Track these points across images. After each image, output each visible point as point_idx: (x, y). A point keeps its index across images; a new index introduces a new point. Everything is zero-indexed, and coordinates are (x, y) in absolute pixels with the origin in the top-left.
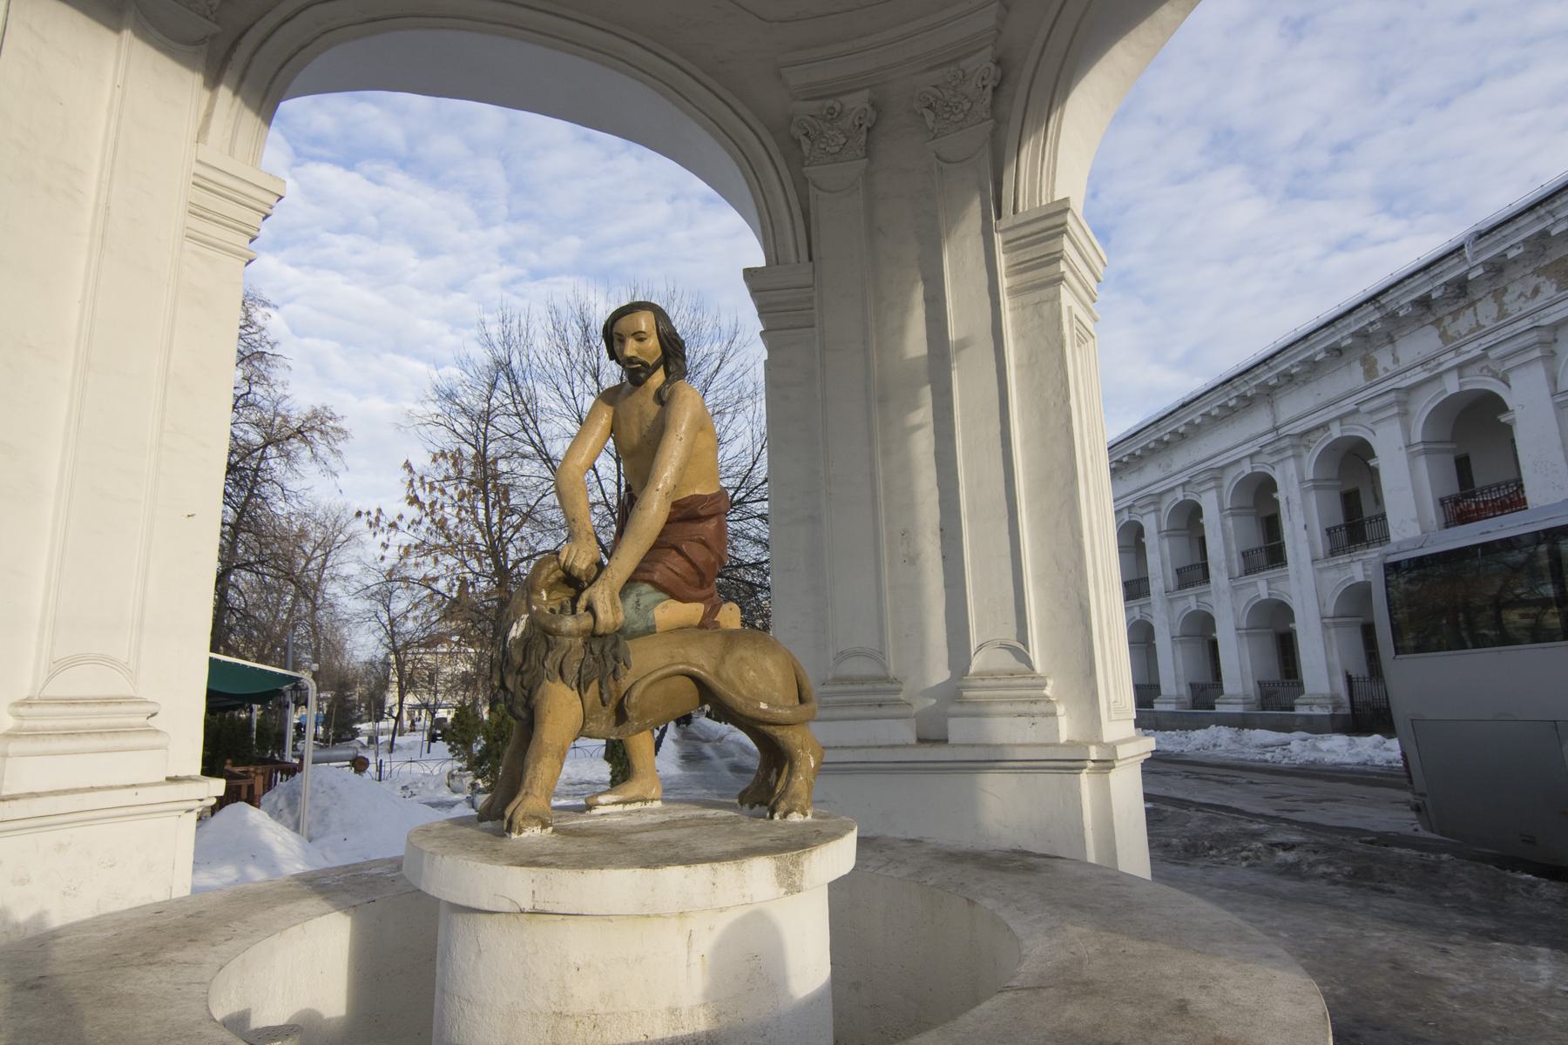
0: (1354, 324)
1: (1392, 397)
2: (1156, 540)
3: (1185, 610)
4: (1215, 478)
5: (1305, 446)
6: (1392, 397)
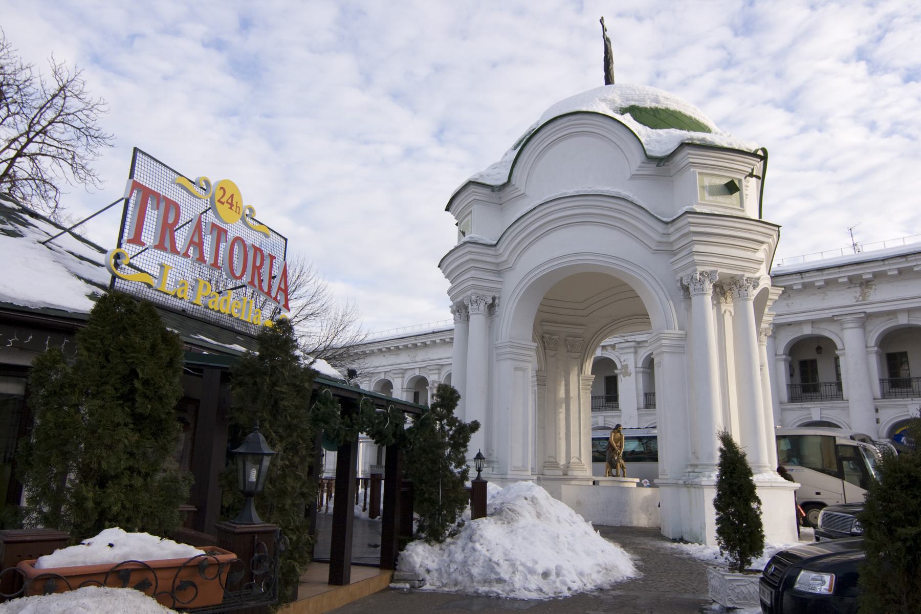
0: (828, 276)
1: (633, 344)
2: (400, 392)
4: (438, 369)
6: (633, 344)
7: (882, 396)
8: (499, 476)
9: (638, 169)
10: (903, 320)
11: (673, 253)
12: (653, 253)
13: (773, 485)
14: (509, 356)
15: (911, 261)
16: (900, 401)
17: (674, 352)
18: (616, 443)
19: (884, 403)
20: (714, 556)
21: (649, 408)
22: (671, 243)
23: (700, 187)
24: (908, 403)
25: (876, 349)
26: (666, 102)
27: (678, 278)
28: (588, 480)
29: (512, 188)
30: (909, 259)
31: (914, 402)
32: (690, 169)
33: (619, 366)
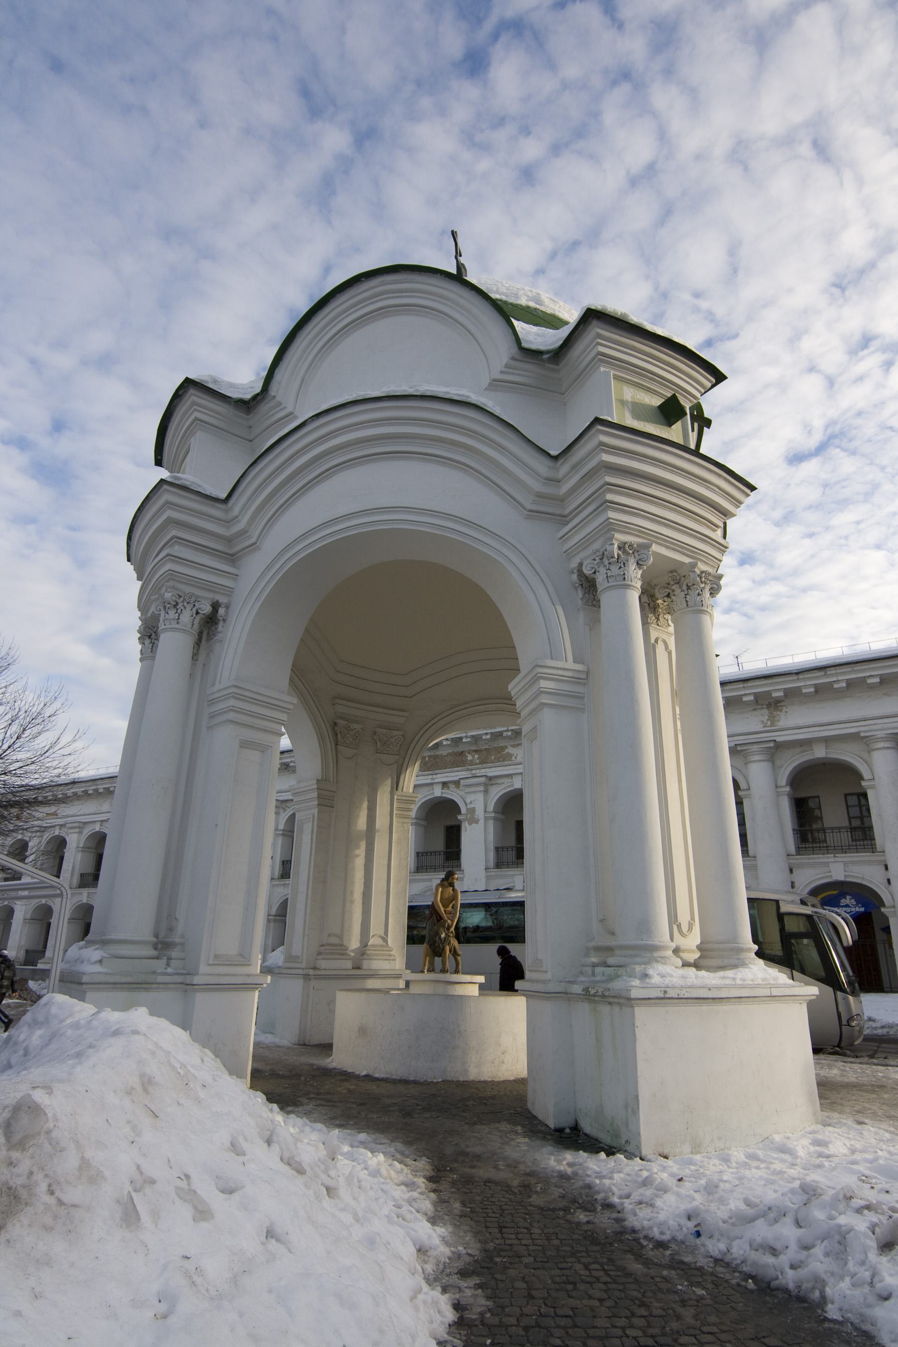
1: (483, 780)
3: (78, 902)
4: (79, 827)
5: (283, 808)
6: (483, 780)
7: (796, 851)
8: (179, 979)
9: (504, 369)
10: (820, 752)
11: (563, 519)
12: (528, 517)
13: (775, 992)
14: (231, 716)
15: (832, 675)
16: (819, 858)
17: (565, 707)
18: (445, 906)
19: (800, 861)
20: (691, 1225)
21: (501, 868)
22: (562, 500)
23: (617, 400)
24: (830, 860)
25: (788, 789)
26: (552, 305)
27: (574, 564)
28: (398, 977)
29: (272, 404)
30: (829, 673)
31: (837, 859)
32: (598, 368)
33: (463, 810)
